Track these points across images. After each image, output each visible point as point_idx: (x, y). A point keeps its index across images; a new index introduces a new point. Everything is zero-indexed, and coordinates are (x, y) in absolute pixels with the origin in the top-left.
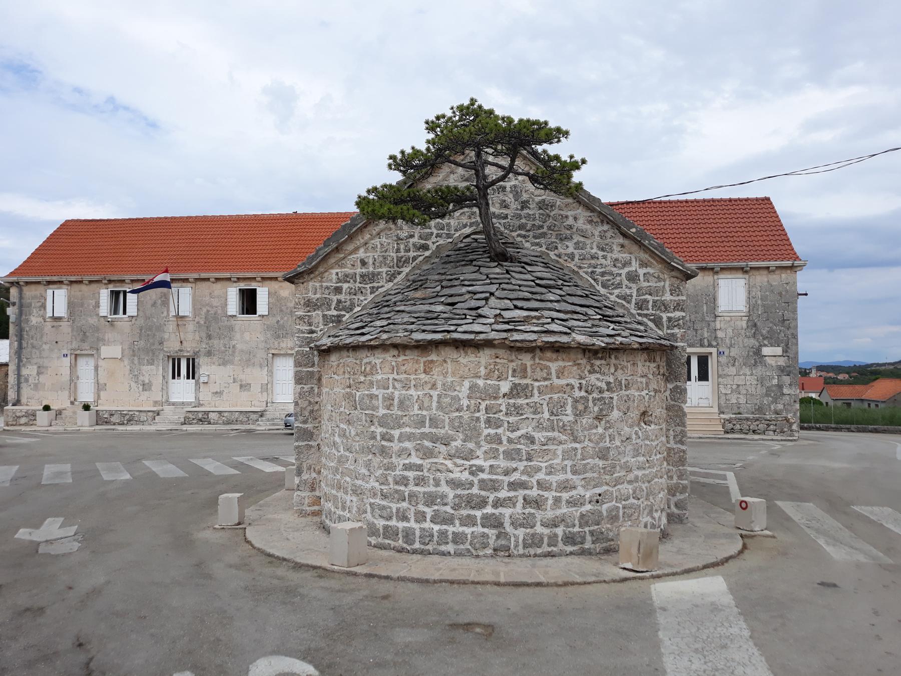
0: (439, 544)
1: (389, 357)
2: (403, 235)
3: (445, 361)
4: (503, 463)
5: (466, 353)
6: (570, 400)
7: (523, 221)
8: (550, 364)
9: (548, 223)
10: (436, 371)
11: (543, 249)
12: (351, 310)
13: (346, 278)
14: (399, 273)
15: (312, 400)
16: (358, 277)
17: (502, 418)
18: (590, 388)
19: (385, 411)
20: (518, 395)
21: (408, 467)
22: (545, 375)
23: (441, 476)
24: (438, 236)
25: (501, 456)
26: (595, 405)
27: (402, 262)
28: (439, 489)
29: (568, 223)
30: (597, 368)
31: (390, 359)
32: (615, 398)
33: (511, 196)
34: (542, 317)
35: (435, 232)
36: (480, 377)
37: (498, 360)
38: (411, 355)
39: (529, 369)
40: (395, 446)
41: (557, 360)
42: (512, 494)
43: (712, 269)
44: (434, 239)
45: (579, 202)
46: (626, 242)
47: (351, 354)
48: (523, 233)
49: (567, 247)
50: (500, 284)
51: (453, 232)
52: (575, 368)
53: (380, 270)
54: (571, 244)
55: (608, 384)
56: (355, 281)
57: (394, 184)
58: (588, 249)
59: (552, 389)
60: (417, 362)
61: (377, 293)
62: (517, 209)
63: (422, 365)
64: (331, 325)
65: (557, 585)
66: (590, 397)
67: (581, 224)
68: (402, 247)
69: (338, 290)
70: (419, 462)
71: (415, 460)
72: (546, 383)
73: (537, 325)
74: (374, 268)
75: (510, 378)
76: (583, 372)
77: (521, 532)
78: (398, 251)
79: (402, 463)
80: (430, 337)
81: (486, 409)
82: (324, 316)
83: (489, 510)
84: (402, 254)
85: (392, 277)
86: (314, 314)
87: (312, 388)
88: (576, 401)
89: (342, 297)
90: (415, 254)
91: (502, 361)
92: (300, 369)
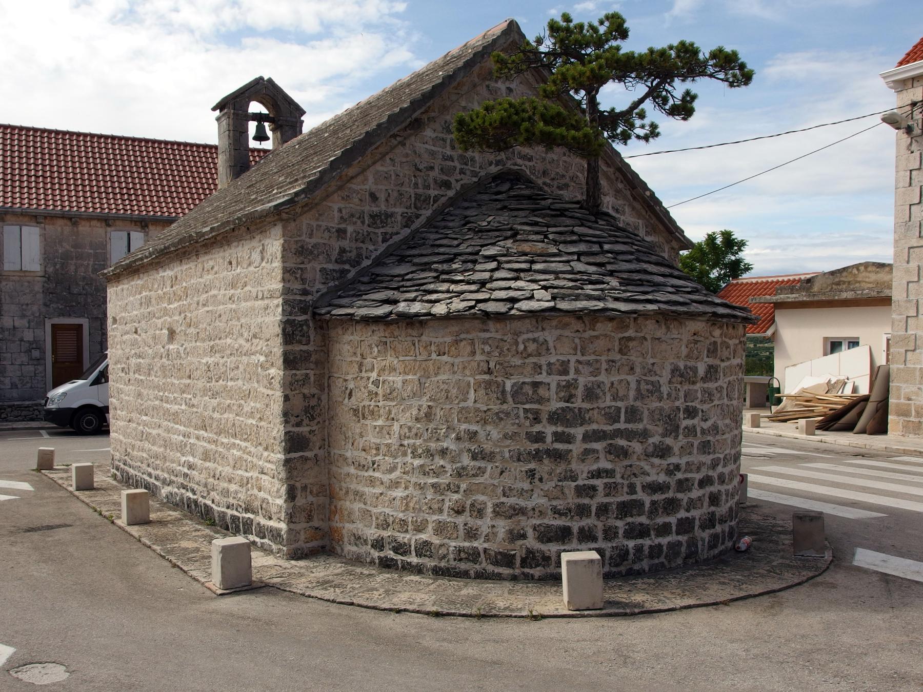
4: (697, 458)
12: (359, 263)
14: (418, 216)
17: (698, 406)
19: (563, 405)
21: (598, 474)
23: (638, 482)
24: (462, 172)
25: (695, 451)
27: (421, 201)
40: (577, 448)
42: (700, 493)
51: (477, 170)
53: (393, 210)
56: (363, 223)
61: (390, 242)
63: (617, 343)
69: (341, 233)
70: (609, 466)
77: (706, 534)
79: (586, 470)
81: (685, 396)
83: (682, 514)
86: (308, 266)
87: (307, 375)
89: (346, 244)
90: (436, 192)
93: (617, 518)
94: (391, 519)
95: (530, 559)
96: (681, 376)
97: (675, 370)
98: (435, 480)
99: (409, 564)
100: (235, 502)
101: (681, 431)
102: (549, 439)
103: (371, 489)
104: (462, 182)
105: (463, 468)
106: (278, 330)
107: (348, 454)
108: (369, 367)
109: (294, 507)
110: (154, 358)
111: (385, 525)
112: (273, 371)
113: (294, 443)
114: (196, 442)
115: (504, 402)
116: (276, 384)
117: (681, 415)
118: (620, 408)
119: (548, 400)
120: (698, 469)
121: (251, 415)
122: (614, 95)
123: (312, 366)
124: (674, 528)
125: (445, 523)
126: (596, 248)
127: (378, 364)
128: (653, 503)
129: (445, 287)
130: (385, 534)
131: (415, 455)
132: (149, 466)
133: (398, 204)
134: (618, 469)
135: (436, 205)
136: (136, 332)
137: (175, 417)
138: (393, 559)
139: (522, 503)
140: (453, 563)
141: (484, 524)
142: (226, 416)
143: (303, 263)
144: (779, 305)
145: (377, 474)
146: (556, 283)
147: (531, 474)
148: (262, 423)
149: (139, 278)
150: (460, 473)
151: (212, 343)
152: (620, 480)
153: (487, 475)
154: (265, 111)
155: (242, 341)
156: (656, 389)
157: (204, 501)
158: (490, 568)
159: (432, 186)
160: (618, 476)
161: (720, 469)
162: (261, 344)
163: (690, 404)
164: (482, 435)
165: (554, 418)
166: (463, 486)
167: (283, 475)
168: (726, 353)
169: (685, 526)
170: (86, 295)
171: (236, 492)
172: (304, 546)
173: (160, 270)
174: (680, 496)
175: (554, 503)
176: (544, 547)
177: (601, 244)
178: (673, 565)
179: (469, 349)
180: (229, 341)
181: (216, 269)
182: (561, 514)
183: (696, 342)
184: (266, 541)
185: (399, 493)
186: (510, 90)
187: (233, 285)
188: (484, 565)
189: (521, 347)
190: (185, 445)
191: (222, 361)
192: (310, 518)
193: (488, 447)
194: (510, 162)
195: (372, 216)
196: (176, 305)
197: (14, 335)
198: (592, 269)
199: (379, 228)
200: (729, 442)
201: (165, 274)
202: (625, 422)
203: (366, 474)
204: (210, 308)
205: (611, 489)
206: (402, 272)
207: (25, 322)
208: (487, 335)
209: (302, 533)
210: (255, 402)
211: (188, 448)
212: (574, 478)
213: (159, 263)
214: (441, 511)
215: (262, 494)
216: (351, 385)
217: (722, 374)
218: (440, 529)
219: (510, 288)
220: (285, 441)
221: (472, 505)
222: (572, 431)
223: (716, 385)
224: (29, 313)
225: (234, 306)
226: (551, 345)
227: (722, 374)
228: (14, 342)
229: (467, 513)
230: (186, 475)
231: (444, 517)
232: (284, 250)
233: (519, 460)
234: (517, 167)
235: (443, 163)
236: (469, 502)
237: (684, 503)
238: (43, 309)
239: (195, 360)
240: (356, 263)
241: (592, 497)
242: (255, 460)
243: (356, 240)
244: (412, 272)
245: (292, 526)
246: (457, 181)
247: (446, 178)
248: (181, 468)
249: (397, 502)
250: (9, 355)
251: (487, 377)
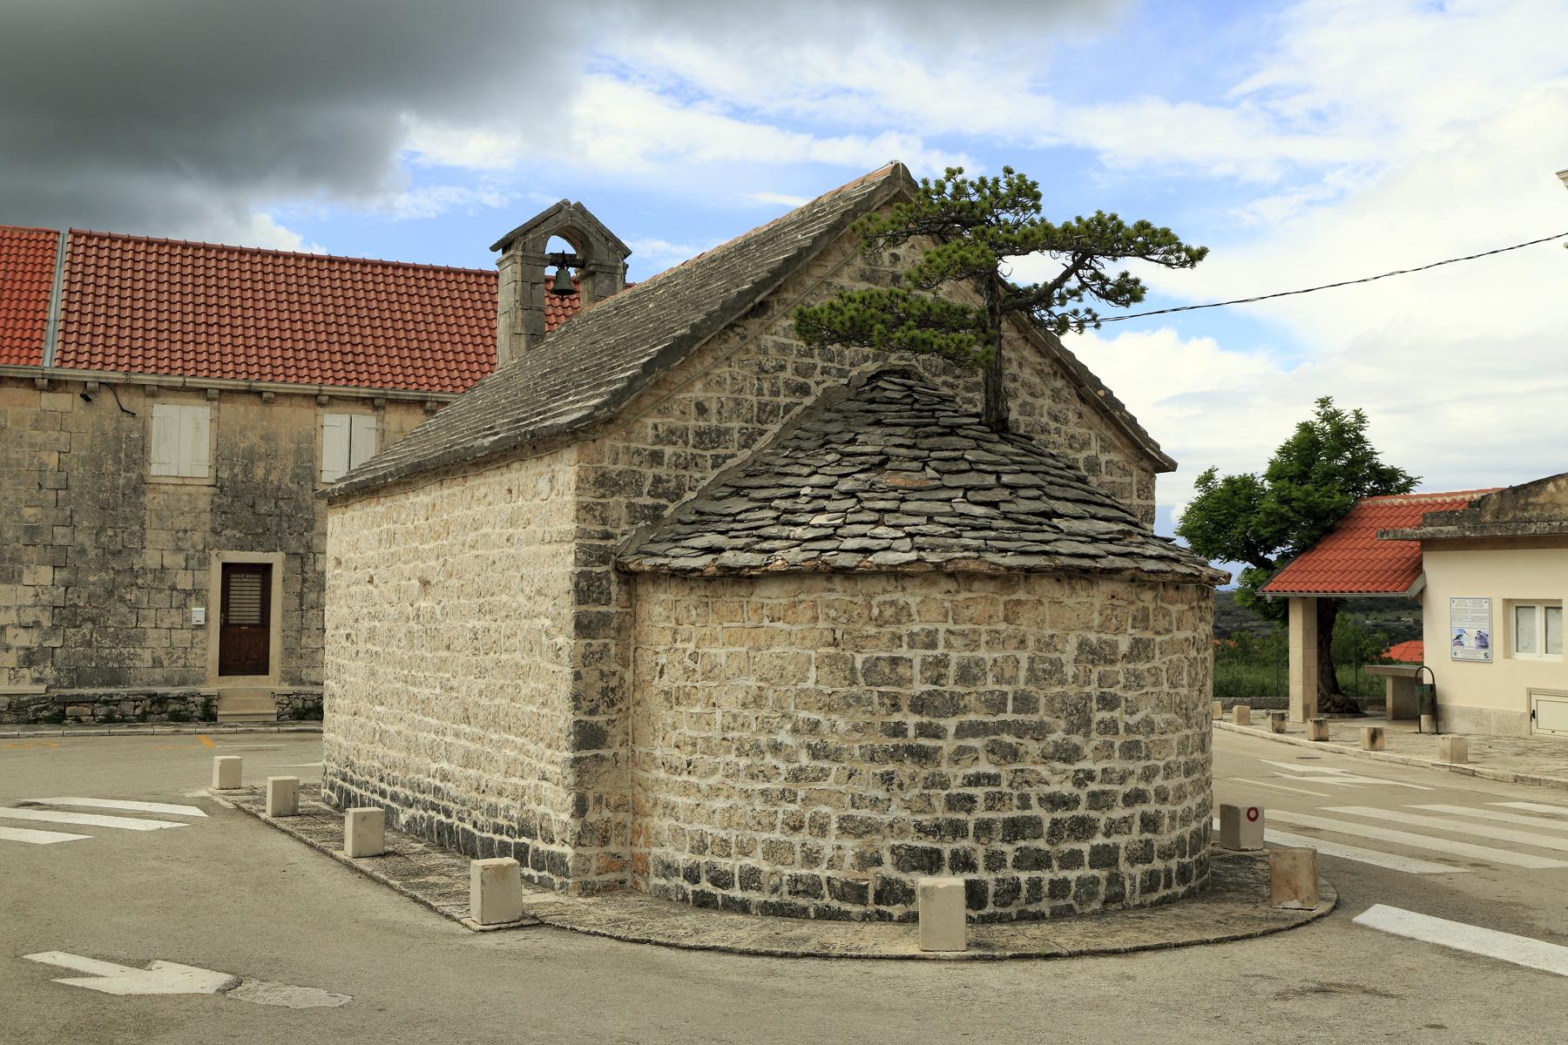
0: (1028, 902)
1: (938, 593)
3: (1040, 602)
4: (1118, 764)
5: (1073, 589)
8: (1170, 607)
12: (679, 497)
13: (671, 436)
15: (605, 668)
17: (1119, 693)
20: (1138, 658)
21: (976, 780)
23: (1033, 792)
24: (825, 371)
25: (1117, 754)
27: (766, 412)
28: (1027, 813)
31: (939, 596)
37: (1115, 602)
38: (981, 590)
40: (948, 745)
42: (1127, 812)
43: (260, 393)
46: (1085, 409)
51: (847, 367)
53: (729, 425)
56: (686, 443)
58: (1037, 417)
60: (993, 602)
61: (724, 467)
63: (1001, 608)
64: (642, 524)
65: (1145, 949)
67: (1027, 374)
68: (766, 385)
69: (656, 458)
70: (992, 770)
71: (985, 767)
74: (720, 421)
75: (1130, 631)
77: (1139, 870)
79: (961, 774)
80: (1010, 560)
81: (1100, 680)
82: (630, 506)
83: (1099, 840)
84: (767, 398)
85: (749, 440)
86: (611, 501)
87: (606, 645)
89: (662, 471)
90: (788, 400)
92: (584, 608)
93: (1003, 840)
94: (709, 839)
95: (890, 892)
96: (1093, 652)
97: (1083, 645)
98: (766, 785)
99: (733, 900)
100: (505, 823)
101: (1094, 726)
102: (911, 732)
103: (685, 799)
105: (801, 770)
106: (569, 585)
107: (657, 753)
108: (685, 635)
109: (584, 825)
110: (396, 621)
111: (700, 848)
112: (561, 640)
113: (587, 737)
114: (454, 740)
115: (854, 683)
116: (564, 654)
117: (1095, 706)
119: (911, 681)
120: (1122, 780)
121: (531, 700)
122: (1026, 270)
123: (613, 633)
124: (1087, 859)
125: (779, 842)
126: (991, 480)
127: (697, 633)
128: (1055, 822)
129: (786, 531)
130: (702, 859)
131: (741, 752)
132: (382, 780)
134: (1003, 774)
136: (371, 581)
137: (424, 705)
138: (711, 894)
139: (876, 816)
140: (788, 898)
141: (828, 845)
142: (497, 701)
143: (603, 496)
144: (1430, 544)
145: (693, 779)
146: (925, 529)
147: (887, 779)
148: (544, 711)
149: (378, 503)
150: (797, 776)
151: (481, 600)
152: (1008, 790)
153: (831, 779)
154: (570, 250)
155: (521, 599)
156: (1057, 666)
157: (462, 825)
158: (835, 904)
160: (1005, 783)
161: (1158, 781)
162: (546, 604)
164: (825, 725)
165: (918, 705)
166: (801, 794)
167: (571, 779)
168: (1162, 624)
169: (1105, 857)
170: (280, 516)
171: (507, 808)
172: (596, 879)
173: (411, 496)
174: (1093, 814)
175: (919, 818)
176: (904, 877)
177: (998, 474)
178: (1088, 910)
179: (810, 614)
180: (504, 598)
181: (490, 498)
182: (927, 834)
183: (1114, 607)
184: (546, 873)
185: (720, 803)
186: (895, 257)
187: (512, 522)
188: (827, 900)
189: (876, 612)
190: (439, 746)
191: (494, 625)
192: (605, 841)
193: (833, 741)
195: (699, 434)
196: (432, 545)
197: (162, 580)
198: (979, 511)
200: (1175, 744)
201: (418, 500)
203: (679, 779)
204: (481, 552)
205: (994, 801)
206: (734, 511)
207: (180, 559)
208: (833, 596)
209: (594, 861)
210: (538, 681)
211: (442, 750)
212: (944, 785)
213: (409, 483)
214: (773, 827)
215: (541, 809)
216: (663, 660)
217: (1157, 651)
218: (772, 851)
219: (865, 535)
220: (576, 733)
221: (812, 819)
222: (942, 722)
223: (1148, 666)
224: (186, 545)
225: (512, 551)
226: (914, 610)
227: (1157, 651)
228: (160, 591)
229: (806, 830)
230: (437, 790)
231: (776, 835)
232: (580, 480)
233: (872, 759)
236: (808, 816)
237: (1102, 824)
238: (211, 539)
239: (457, 623)
240: (676, 495)
241: (969, 811)
242: (534, 761)
244: (746, 511)
245: (580, 850)
246: (818, 383)
247: (801, 380)
248: (430, 780)
249: (717, 817)
250: (153, 612)
251: (832, 650)
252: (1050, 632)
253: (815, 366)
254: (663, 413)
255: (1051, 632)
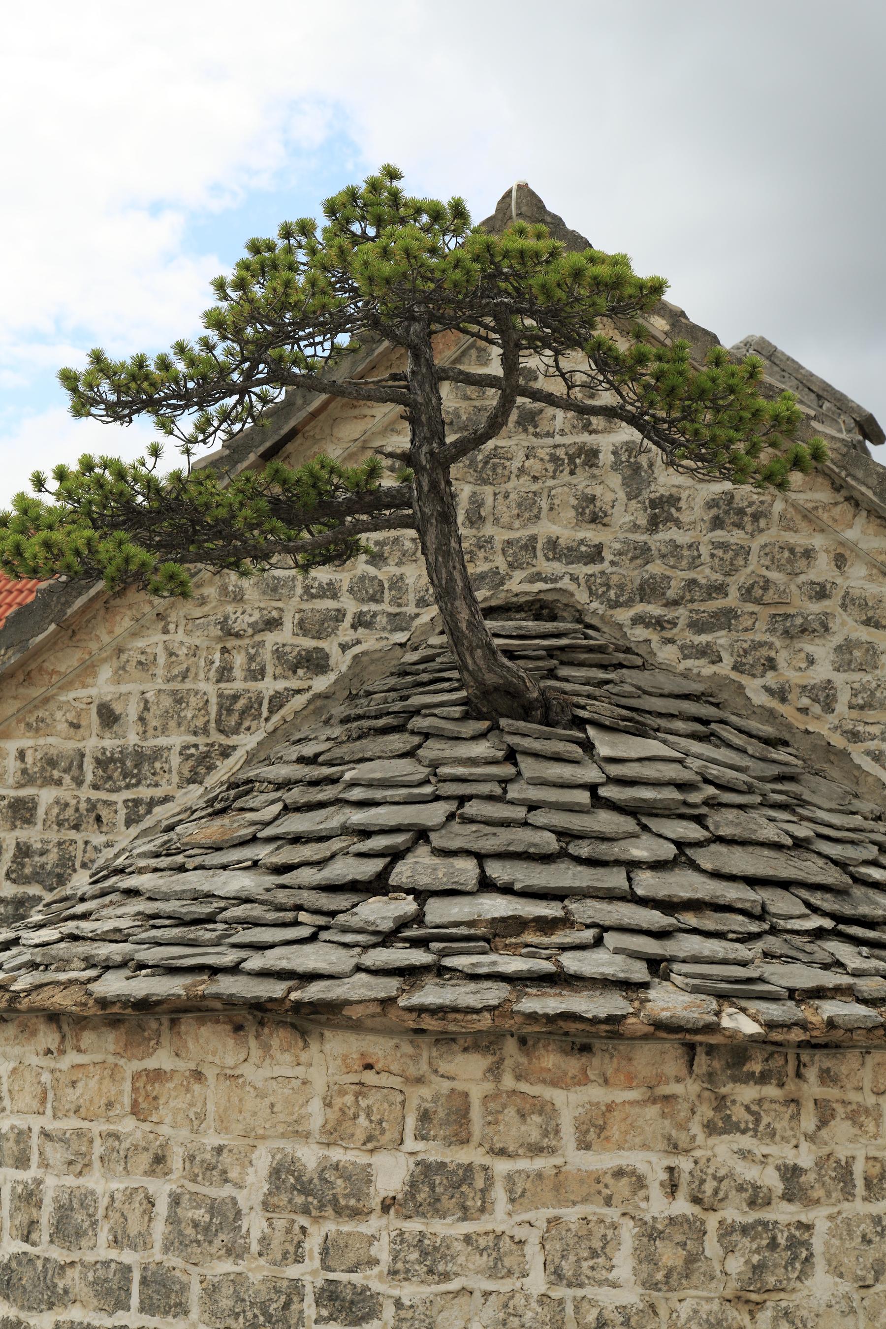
2: (244, 619)
3: (198, 1075)
5: (266, 1048)
6: (628, 1231)
7: (656, 568)
8: (557, 1096)
9: (742, 578)
10: (173, 1102)
11: (725, 668)
12: (62, 880)
14: (226, 752)
16: (89, 766)
17: (376, 1286)
18: (709, 1187)
20: (435, 1208)
22: (535, 1135)
24: (360, 622)
26: (730, 1250)
27: (234, 713)
29: (813, 575)
30: (739, 1114)
31: (35, 1060)
32: (822, 1226)
33: (615, 480)
34: (565, 922)
35: (351, 606)
36: (307, 1135)
37: (369, 1077)
38: (99, 1046)
39: (476, 1113)
41: (583, 1080)
44: (345, 633)
45: (854, 502)
47: (278, 1038)
48: (654, 610)
49: (811, 661)
50: (463, 800)
52: (653, 1111)
53: (162, 741)
54: (822, 650)
55: (791, 1174)
56: (79, 782)
57: (728, 341)
59: (558, 1184)
60: (114, 1072)
61: (148, 822)
62: (635, 527)
63: (127, 1086)
66: (712, 1222)
68: (239, 660)
72: (540, 1163)
73: (533, 950)
76: (683, 1127)
78: (224, 673)
81: (325, 1252)
84: (238, 685)
88: (651, 1234)
89: (32, 835)
90: (281, 685)
91: (384, 1080)
96: (305, 1189)
97: (282, 1173)
104: (357, 650)
118: (129, 1269)
133: (172, 724)
135: (276, 718)
156: (225, 1216)
159: (270, 670)
163: (343, 1277)
194: (518, 575)
195: (102, 763)
199: (118, 790)
202: (142, 1310)
234: (540, 586)
235: (306, 606)
243: (60, 824)
246: (344, 647)
247: (309, 643)
252: (213, 1140)
253: (340, 615)
254: (37, 728)
255: (217, 1141)
